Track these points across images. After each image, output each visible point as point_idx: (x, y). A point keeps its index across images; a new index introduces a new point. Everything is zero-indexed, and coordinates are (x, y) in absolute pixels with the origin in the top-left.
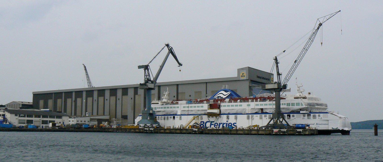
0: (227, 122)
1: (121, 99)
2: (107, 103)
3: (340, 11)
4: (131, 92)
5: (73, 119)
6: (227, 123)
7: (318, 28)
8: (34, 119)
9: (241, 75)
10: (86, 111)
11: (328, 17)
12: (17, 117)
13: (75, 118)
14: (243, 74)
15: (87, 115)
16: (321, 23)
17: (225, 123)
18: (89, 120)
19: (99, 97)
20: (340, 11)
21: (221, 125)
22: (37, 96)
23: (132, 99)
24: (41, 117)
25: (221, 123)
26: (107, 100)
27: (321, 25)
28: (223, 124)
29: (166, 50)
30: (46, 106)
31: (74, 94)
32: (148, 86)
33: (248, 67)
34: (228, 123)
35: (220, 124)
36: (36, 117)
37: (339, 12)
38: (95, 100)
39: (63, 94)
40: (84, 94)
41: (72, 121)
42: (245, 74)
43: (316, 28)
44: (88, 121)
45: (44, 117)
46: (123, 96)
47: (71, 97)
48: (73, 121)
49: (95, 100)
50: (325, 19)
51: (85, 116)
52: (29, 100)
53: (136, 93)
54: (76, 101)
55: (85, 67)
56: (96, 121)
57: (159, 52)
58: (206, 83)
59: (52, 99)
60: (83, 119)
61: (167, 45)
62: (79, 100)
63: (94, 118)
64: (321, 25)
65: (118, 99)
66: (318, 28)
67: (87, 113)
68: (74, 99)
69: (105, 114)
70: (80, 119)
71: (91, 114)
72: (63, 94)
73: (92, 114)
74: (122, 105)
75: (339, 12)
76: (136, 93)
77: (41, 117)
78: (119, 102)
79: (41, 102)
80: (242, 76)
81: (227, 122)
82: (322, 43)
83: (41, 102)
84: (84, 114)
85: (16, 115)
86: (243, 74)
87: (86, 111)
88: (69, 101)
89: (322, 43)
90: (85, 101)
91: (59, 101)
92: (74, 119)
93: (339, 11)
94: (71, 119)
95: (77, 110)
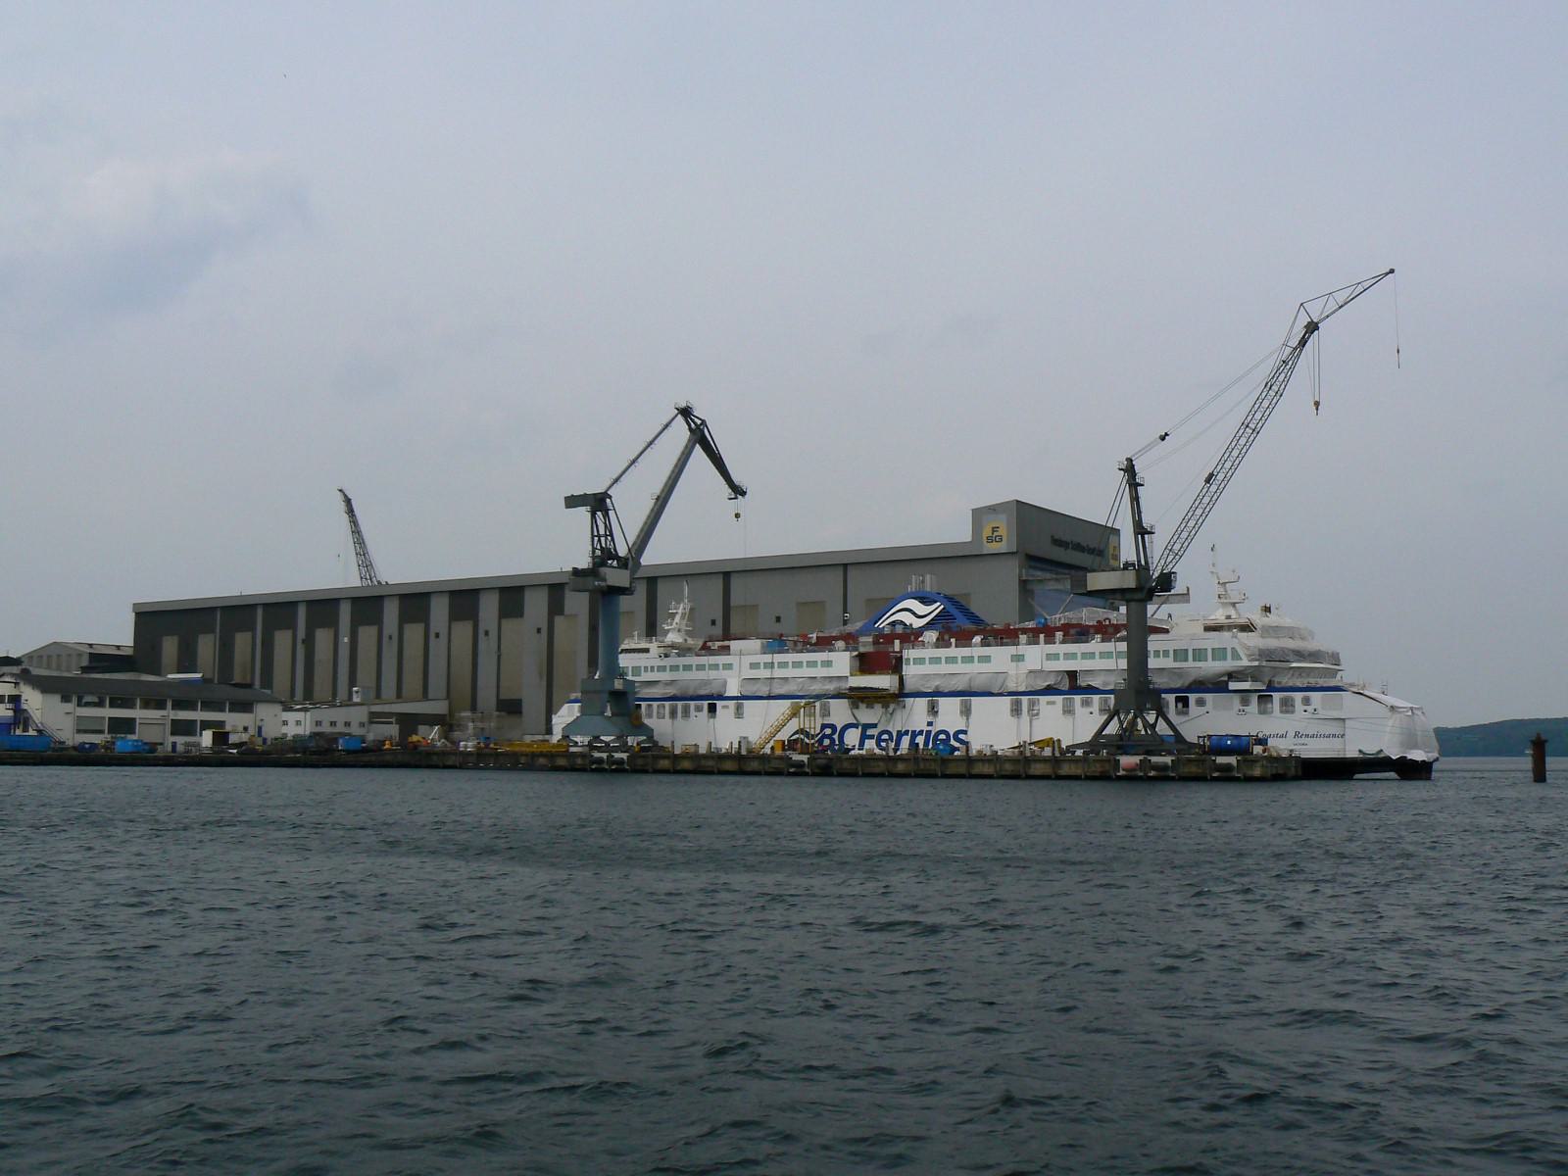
0: (930, 728)
1: (493, 634)
2: (438, 648)
3: (1392, 271)
4: (536, 605)
5: (300, 716)
6: (929, 733)
7: (1303, 343)
8: (137, 713)
9: (987, 532)
10: (352, 682)
11: (1341, 297)
12: (69, 707)
13: (305, 710)
14: (994, 529)
15: (356, 699)
16: (1315, 320)
17: (921, 732)
18: (365, 719)
19: (453, 626)
20: (1392, 271)
21: (906, 741)
22: (151, 621)
23: (713, 623)
24: (169, 704)
25: (907, 732)
26: (437, 635)
27: (1312, 327)
28: (914, 734)
29: (681, 432)
30: (187, 662)
31: (302, 612)
32: (605, 580)
33: (1017, 501)
34: (934, 730)
35: (900, 734)
36: (146, 705)
37: (1387, 274)
38: (390, 637)
39: (260, 612)
40: (345, 612)
41: (295, 724)
42: (1003, 531)
43: (1294, 342)
44: (362, 725)
45: (179, 705)
46: (504, 622)
47: (292, 626)
48: (298, 723)
49: (390, 637)
50: (1332, 306)
51: (349, 703)
52: (121, 635)
53: (556, 607)
54: (309, 641)
55: (348, 501)
56: (391, 723)
57: (651, 439)
58: (841, 568)
59: (288, 628)
60: (339, 715)
61: (686, 412)
62: (323, 637)
63: (387, 709)
64: (1312, 327)
65: (385, 639)
66: (1303, 343)
67: (355, 689)
68: (301, 633)
69: (430, 697)
70: (327, 715)
71: (372, 694)
72: (260, 612)
73: (378, 695)
74: (499, 657)
75: (1387, 274)
76: (556, 607)
77: (169, 704)
78: (487, 646)
79: (170, 646)
80: (990, 540)
81: (930, 728)
82: (1317, 404)
83: (170, 646)
84: (342, 694)
85: (66, 699)
86: (993, 528)
87: (352, 682)
88: (282, 640)
89: (1317, 404)
90: (346, 640)
91: (242, 640)
92: (303, 713)
93: (1388, 270)
94: (291, 716)
95: (317, 680)
